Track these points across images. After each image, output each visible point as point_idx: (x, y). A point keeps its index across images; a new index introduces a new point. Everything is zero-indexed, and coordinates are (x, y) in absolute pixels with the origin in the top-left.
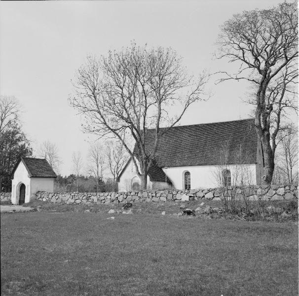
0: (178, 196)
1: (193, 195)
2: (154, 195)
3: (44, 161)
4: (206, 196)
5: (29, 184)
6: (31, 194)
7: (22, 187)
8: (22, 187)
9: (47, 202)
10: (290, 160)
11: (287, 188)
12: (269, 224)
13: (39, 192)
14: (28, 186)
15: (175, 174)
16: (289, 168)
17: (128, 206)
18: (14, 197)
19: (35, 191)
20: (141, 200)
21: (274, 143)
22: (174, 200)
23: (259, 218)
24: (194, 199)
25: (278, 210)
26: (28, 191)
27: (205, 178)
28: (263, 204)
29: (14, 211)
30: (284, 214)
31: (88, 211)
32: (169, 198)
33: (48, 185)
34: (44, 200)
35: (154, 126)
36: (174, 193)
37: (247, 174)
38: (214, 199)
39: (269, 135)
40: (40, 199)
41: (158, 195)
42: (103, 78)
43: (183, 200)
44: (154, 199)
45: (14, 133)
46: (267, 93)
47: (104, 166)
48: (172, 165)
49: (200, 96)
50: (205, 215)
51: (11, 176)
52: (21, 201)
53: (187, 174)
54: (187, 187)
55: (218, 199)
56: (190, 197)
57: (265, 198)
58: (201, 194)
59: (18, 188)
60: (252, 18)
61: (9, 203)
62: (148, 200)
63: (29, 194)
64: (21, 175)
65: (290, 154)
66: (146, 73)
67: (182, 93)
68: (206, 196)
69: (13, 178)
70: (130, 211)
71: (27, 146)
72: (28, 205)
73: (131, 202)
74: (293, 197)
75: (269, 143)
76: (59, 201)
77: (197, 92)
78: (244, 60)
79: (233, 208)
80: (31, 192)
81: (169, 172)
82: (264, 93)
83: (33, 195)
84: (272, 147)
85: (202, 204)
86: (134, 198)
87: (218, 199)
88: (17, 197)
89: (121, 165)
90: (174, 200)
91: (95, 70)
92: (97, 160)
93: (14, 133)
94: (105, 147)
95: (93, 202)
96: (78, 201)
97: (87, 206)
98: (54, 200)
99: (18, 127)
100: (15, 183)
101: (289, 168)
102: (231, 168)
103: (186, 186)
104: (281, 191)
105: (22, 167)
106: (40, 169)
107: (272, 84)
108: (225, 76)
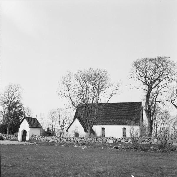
0: (108, 141)
1: (115, 140)
2: (96, 139)
3: (36, 119)
4: (121, 141)
5: (29, 131)
6: (30, 136)
7: (25, 132)
8: (25, 132)
9: (38, 140)
10: (156, 124)
11: (159, 139)
12: (153, 153)
13: (33, 135)
14: (28, 131)
15: (97, 129)
16: (155, 129)
17: (83, 144)
18: (20, 138)
19: (31, 135)
20: (89, 142)
21: (153, 118)
22: (106, 142)
23: (148, 151)
24: (115, 142)
25: (155, 148)
26: (19, 136)
27: (114, 132)
28: (149, 146)
29: (26, 144)
30: (158, 150)
31: (63, 146)
32: (103, 141)
33: (37, 132)
34: (37, 139)
35: (91, 102)
36: (106, 139)
37: (133, 131)
38: (125, 143)
39: (151, 114)
40: (34, 139)
41: (97, 140)
42: (74, 82)
43: (110, 142)
44: (96, 141)
45: (17, 103)
46: (151, 95)
47: (57, 122)
48: (96, 124)
49: (117, 92)
50: (123, 150)
51: (18, 126)
52: (24, 139)
53: (103, 129)
54: (103, 135)
55: (127, 143)
56: (114, 141)
57: (148, 143)
58: (119, 140)
59: (22, 133)
60: (145, 61)
61: (16, 140)
62: (93, 142)
63: (29, 136)
64: (25, 126)
65: (156, 121)
66: (96, 81)
67: (109, 91)
68: (121, 141)
69: (19, 127)
70: (85, 147)
71: (22, 110)
72: (27, 141)
73: (84, 142)
74: (161, 143)
75: (151, 118)
76: (45, 140)
77: (116, 90)
78: (141, 80)
79: (136, 146)
80: (30, 135)
81: (95, 128)
82: (149, 95)
83: (30, 137)
84: (151, 119)
85: (120, 145)
86: (85, 140)
87: (127, 143)
88: (21, 137)
89: (66, 122)
90: (106, 142)
91: (70, 79)
92: (53, 118)
93: (17, 103)
94: (57, 112)
95: (64, 142)
96: (56, 141)
97: (61, 143)
98: (42, 140)
99: (19, 100)
100: (21, 130)
101: (155, 129)
102: (127, 127)
103: (124, 136)
104: (156, 140)
105: (25, 121)
106: (34, 123)
107: (154, 91)
108: (132, 87)
